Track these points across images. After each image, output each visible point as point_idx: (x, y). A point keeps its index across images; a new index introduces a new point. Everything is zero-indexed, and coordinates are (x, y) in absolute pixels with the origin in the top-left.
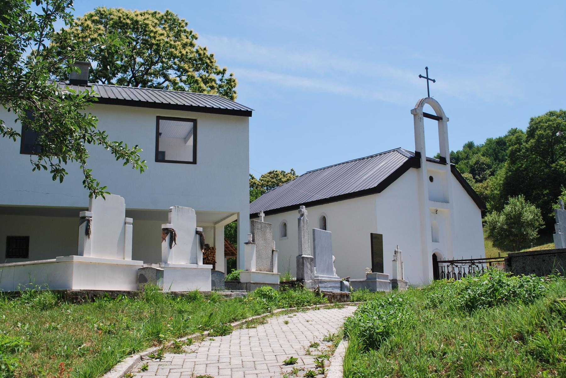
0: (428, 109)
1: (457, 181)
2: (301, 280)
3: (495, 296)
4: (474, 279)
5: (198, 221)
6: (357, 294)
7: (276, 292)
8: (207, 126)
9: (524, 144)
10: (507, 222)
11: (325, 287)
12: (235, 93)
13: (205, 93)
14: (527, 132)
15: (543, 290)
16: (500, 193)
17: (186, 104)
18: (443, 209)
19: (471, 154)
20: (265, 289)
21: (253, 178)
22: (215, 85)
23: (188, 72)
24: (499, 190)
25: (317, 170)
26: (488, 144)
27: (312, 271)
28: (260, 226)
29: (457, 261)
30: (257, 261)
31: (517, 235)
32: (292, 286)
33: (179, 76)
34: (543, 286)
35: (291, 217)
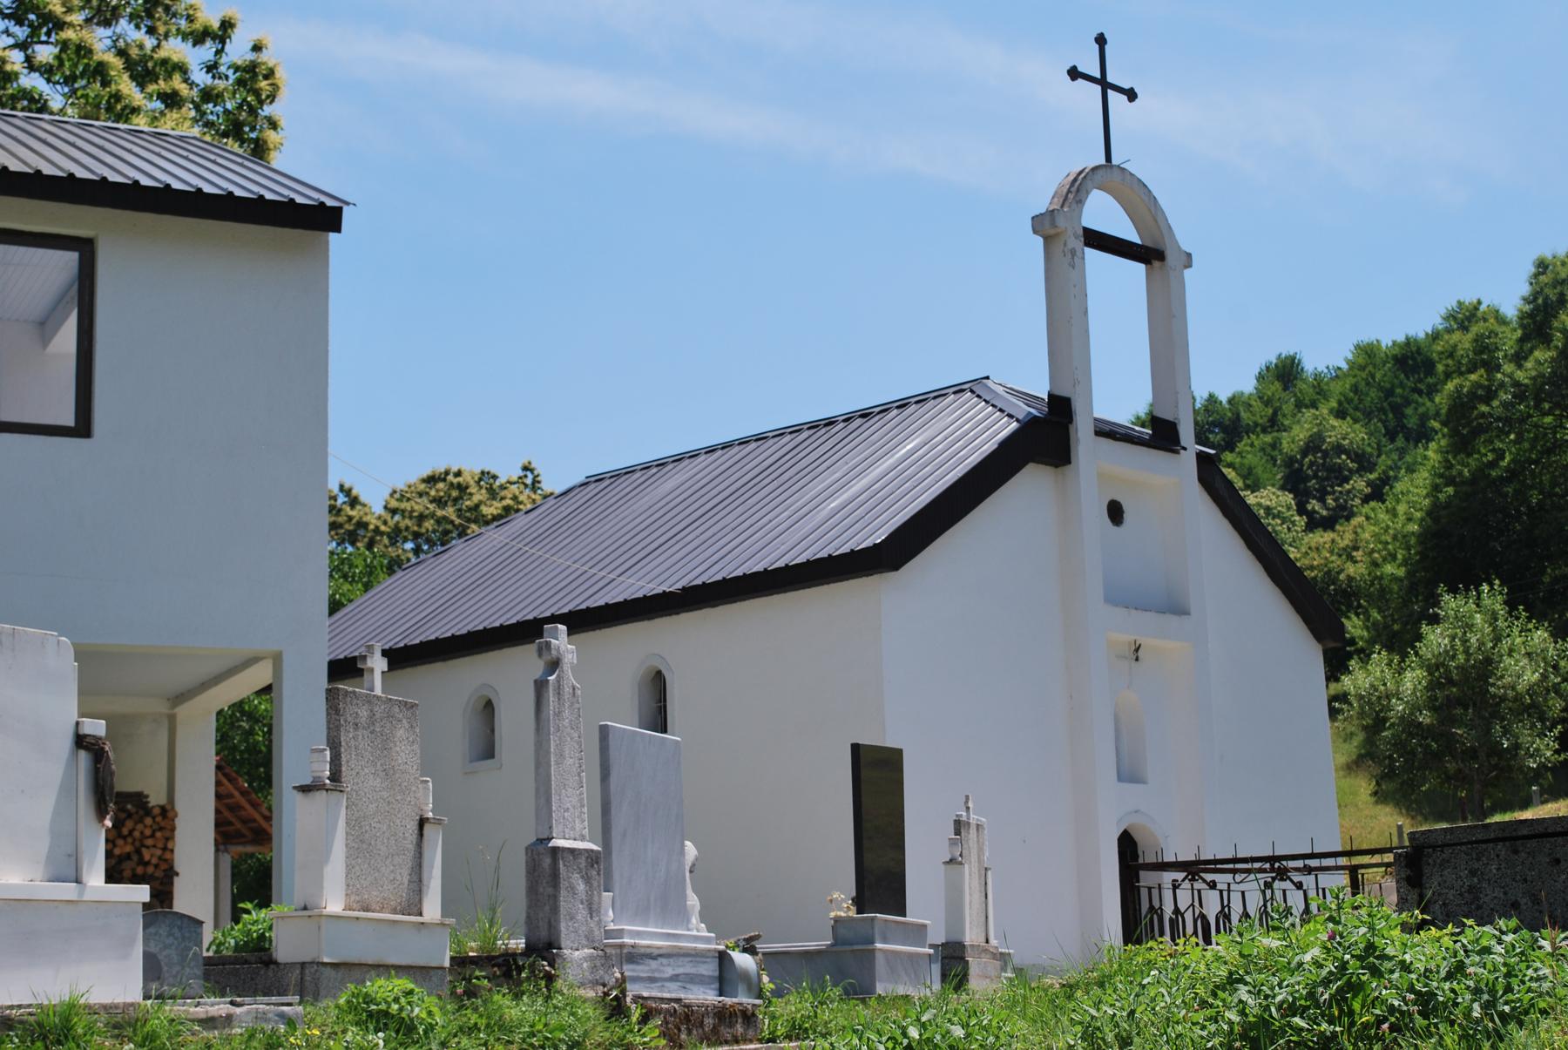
0: (1104, 213)
1: (1225, 523)
2: (544, 948)
3: (1351, 1013)
4: (1266, 941)
5: (82, 693)
6: (792, 1007)
7: (432, 1001)
8: (143, 275)
9: (1508, 368)
10: (1433, 699)
11: (652, 980)
12: (274, 125)
13: (141, 122)
14: (1523, 316)
15: (1546, 985)
16: (1410, 574)
17: (48, 170)
18: (1166, 642)
19: (1288, 408)
20: (383, 988)
21: (354, 502)
22: (183, 89)
23: (60, 25)
24: (1405, 563)
25: (630, 471)
26: (1362, 368)
27: (593, 909)
28: (364, 713)
29: (1215, 865)
30: (349, 869)
31: (1472, 754)
32: (507, 975)
33: (22, 46)
34: (1547, 971)
35: (509, 672)
